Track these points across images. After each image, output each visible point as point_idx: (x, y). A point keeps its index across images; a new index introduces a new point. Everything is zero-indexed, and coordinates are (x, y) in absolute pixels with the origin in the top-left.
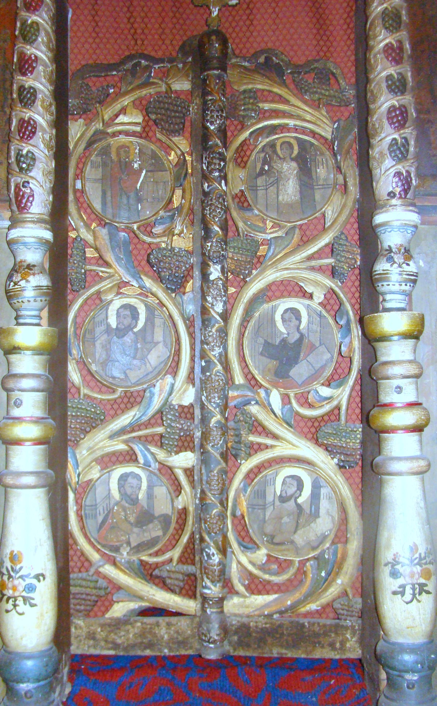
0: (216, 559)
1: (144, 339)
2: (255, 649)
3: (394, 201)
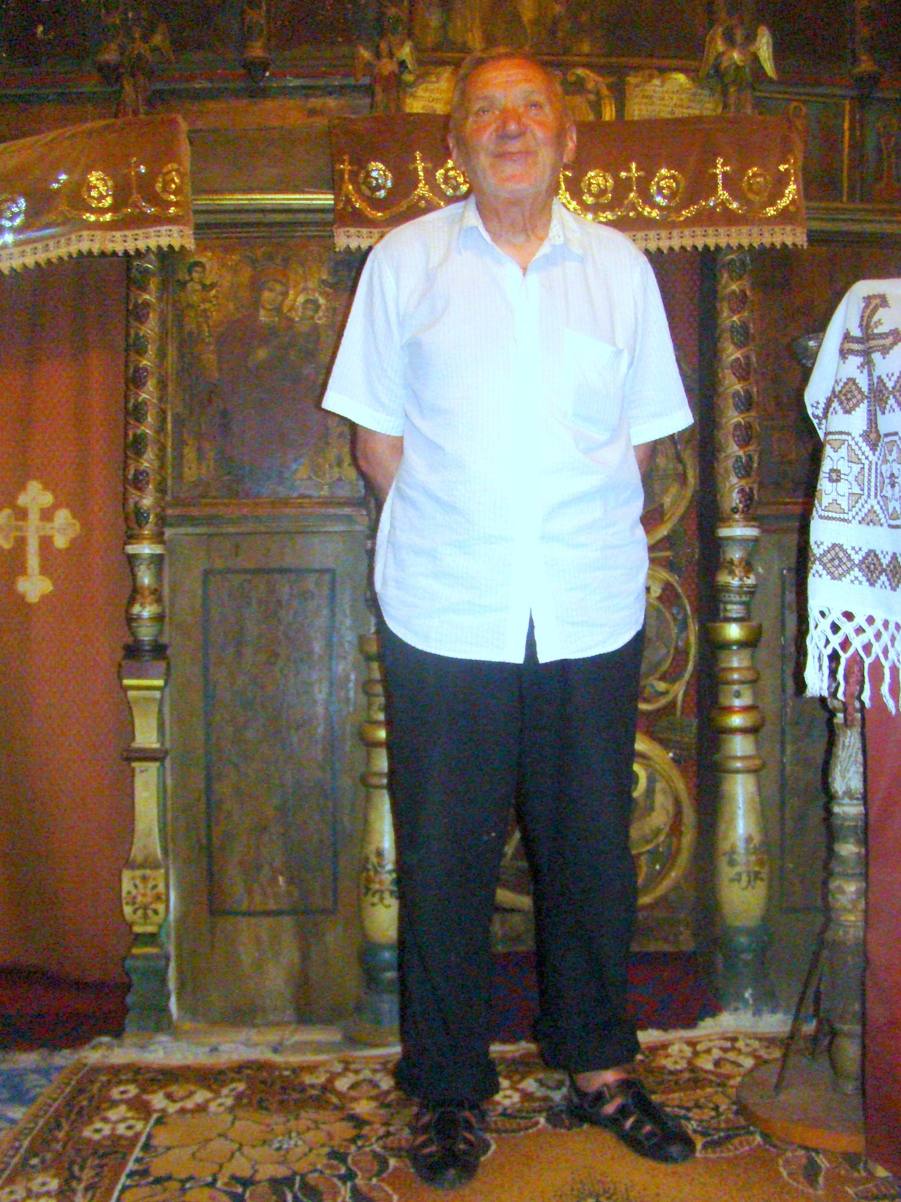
3: (737, 516)
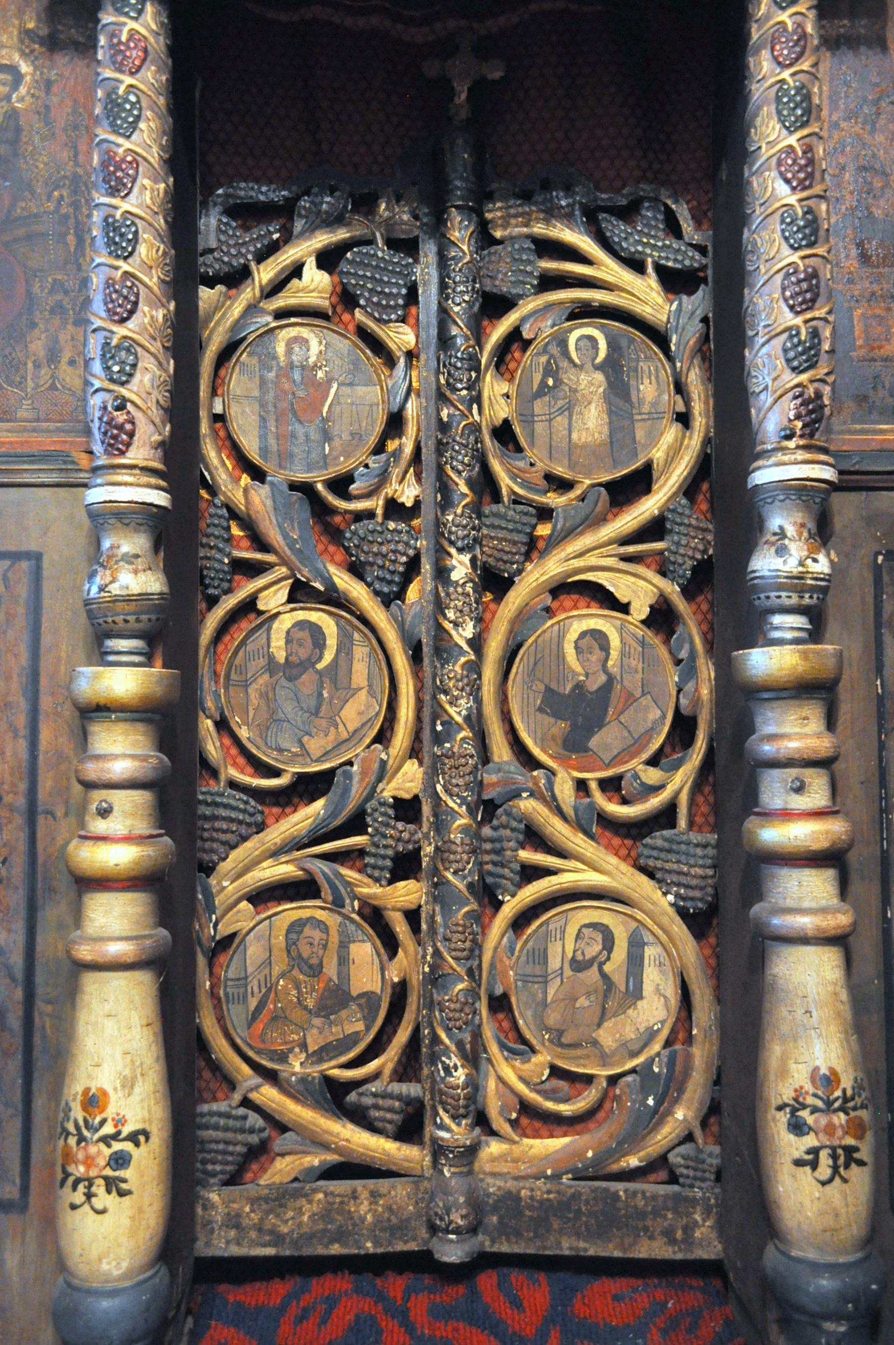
0: (460, 1075)
1: (334, 682)
2: (530, 1239)
